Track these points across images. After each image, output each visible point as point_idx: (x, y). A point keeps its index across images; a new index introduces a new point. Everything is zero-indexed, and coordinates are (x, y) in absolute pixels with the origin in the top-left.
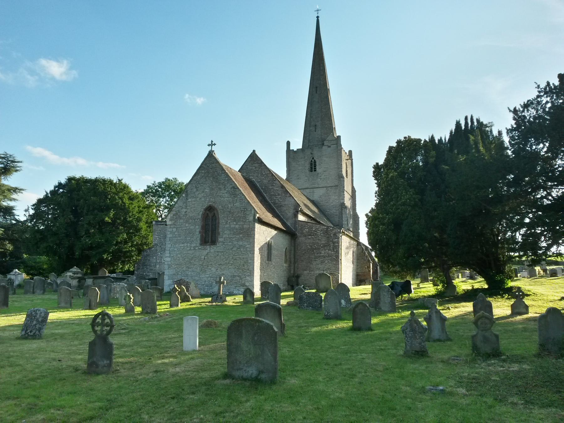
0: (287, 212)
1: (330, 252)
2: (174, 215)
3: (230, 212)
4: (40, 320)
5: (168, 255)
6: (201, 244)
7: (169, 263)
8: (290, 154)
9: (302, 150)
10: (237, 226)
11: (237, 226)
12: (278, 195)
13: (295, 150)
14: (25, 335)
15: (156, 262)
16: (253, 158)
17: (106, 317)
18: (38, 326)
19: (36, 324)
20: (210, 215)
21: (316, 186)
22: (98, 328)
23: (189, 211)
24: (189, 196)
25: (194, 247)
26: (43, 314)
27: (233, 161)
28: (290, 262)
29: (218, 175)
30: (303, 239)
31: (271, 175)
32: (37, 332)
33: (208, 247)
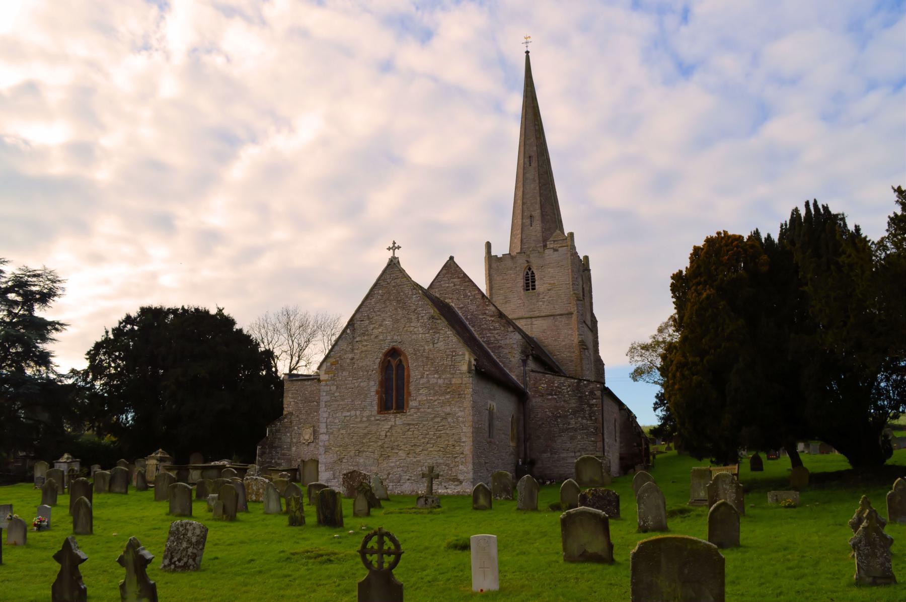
0: (509, 356)
1: (584, 421)
2: (332, 364)
3: (427, 358)
4: (194, 540)
5: (325, 430)
6: (380, 412)
7: (327, 443)
8: (492, 261)
9: (509, 257)
10: (440, 381)
11: (440, 381)
12: (495, 330)
13: (500, 256)
14: (169, 565)
15: (292, 441)
16: (769, 236)
17: (386, 538)
18: (190, 550)
19: (187, 548)
20: (394, 363)
21: (537, 314)
22: (374, 558)
23: (357, 357)
24: (359, 332)
25: (368, 417)
26: (198, 532)
27: (423, 273)
28: (519, 439)
29: (407, 297)
30: (539, 400)
31: (480, 296)
32: (191, 561)
33: (392, 416)
